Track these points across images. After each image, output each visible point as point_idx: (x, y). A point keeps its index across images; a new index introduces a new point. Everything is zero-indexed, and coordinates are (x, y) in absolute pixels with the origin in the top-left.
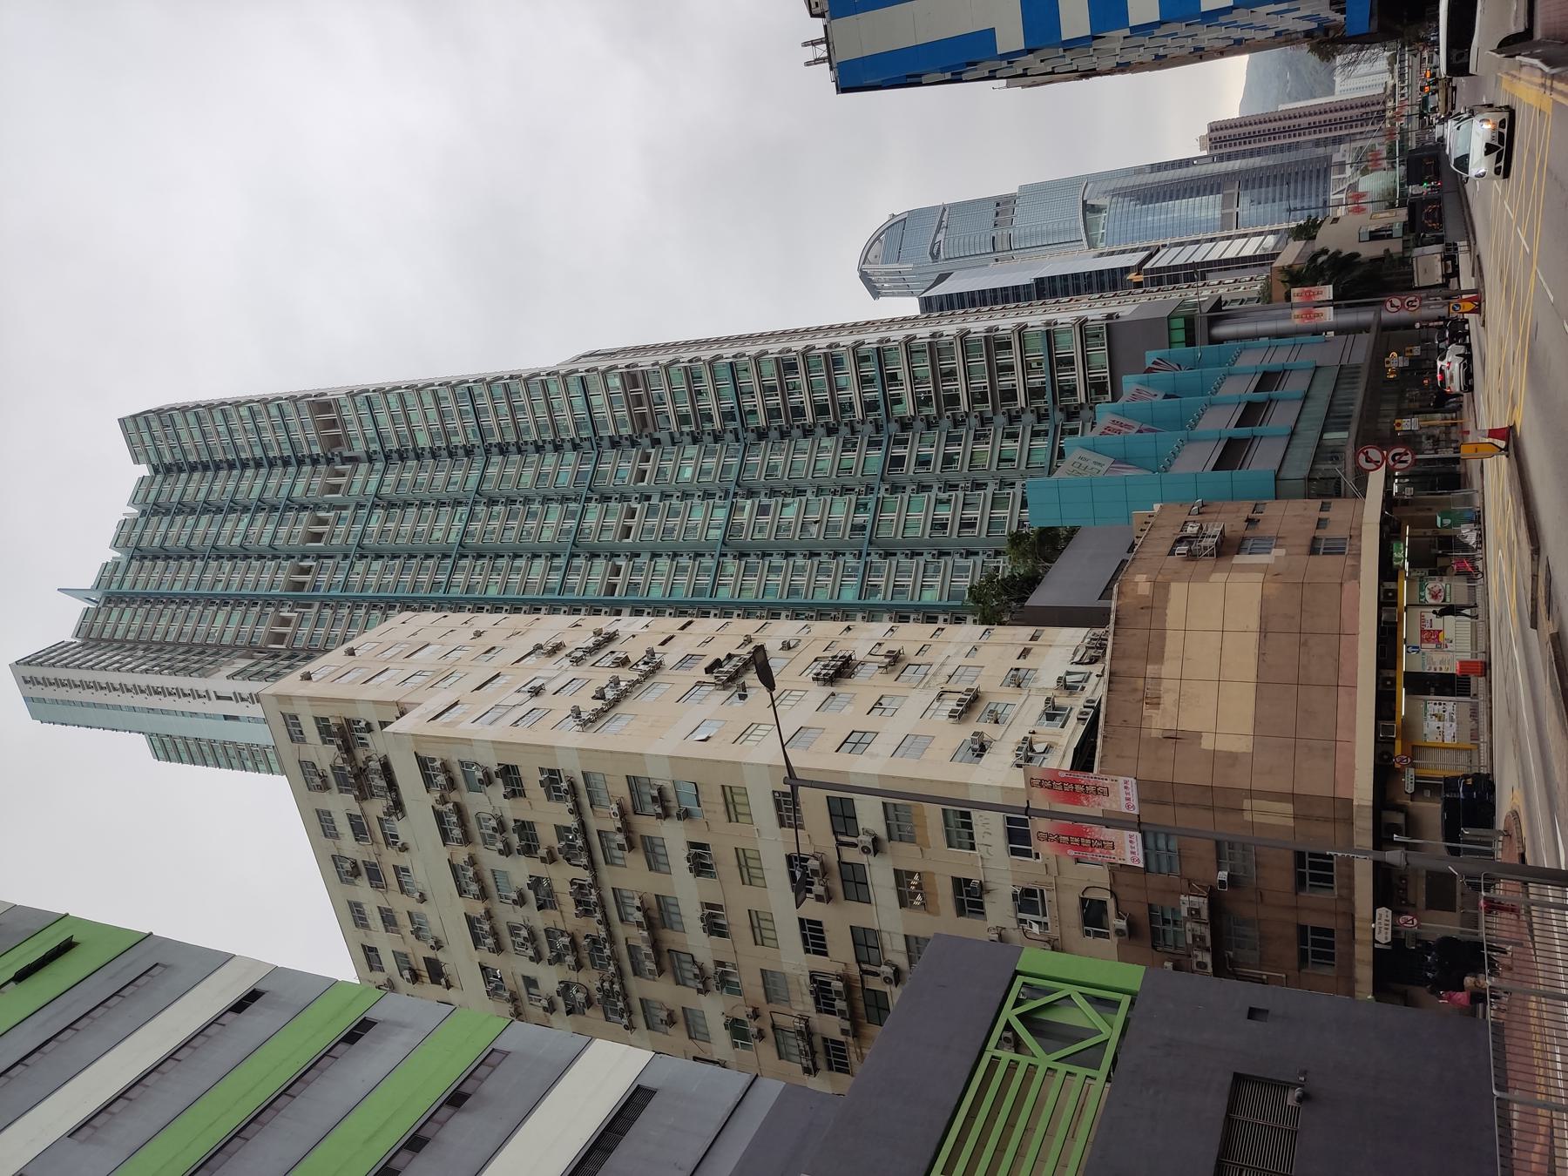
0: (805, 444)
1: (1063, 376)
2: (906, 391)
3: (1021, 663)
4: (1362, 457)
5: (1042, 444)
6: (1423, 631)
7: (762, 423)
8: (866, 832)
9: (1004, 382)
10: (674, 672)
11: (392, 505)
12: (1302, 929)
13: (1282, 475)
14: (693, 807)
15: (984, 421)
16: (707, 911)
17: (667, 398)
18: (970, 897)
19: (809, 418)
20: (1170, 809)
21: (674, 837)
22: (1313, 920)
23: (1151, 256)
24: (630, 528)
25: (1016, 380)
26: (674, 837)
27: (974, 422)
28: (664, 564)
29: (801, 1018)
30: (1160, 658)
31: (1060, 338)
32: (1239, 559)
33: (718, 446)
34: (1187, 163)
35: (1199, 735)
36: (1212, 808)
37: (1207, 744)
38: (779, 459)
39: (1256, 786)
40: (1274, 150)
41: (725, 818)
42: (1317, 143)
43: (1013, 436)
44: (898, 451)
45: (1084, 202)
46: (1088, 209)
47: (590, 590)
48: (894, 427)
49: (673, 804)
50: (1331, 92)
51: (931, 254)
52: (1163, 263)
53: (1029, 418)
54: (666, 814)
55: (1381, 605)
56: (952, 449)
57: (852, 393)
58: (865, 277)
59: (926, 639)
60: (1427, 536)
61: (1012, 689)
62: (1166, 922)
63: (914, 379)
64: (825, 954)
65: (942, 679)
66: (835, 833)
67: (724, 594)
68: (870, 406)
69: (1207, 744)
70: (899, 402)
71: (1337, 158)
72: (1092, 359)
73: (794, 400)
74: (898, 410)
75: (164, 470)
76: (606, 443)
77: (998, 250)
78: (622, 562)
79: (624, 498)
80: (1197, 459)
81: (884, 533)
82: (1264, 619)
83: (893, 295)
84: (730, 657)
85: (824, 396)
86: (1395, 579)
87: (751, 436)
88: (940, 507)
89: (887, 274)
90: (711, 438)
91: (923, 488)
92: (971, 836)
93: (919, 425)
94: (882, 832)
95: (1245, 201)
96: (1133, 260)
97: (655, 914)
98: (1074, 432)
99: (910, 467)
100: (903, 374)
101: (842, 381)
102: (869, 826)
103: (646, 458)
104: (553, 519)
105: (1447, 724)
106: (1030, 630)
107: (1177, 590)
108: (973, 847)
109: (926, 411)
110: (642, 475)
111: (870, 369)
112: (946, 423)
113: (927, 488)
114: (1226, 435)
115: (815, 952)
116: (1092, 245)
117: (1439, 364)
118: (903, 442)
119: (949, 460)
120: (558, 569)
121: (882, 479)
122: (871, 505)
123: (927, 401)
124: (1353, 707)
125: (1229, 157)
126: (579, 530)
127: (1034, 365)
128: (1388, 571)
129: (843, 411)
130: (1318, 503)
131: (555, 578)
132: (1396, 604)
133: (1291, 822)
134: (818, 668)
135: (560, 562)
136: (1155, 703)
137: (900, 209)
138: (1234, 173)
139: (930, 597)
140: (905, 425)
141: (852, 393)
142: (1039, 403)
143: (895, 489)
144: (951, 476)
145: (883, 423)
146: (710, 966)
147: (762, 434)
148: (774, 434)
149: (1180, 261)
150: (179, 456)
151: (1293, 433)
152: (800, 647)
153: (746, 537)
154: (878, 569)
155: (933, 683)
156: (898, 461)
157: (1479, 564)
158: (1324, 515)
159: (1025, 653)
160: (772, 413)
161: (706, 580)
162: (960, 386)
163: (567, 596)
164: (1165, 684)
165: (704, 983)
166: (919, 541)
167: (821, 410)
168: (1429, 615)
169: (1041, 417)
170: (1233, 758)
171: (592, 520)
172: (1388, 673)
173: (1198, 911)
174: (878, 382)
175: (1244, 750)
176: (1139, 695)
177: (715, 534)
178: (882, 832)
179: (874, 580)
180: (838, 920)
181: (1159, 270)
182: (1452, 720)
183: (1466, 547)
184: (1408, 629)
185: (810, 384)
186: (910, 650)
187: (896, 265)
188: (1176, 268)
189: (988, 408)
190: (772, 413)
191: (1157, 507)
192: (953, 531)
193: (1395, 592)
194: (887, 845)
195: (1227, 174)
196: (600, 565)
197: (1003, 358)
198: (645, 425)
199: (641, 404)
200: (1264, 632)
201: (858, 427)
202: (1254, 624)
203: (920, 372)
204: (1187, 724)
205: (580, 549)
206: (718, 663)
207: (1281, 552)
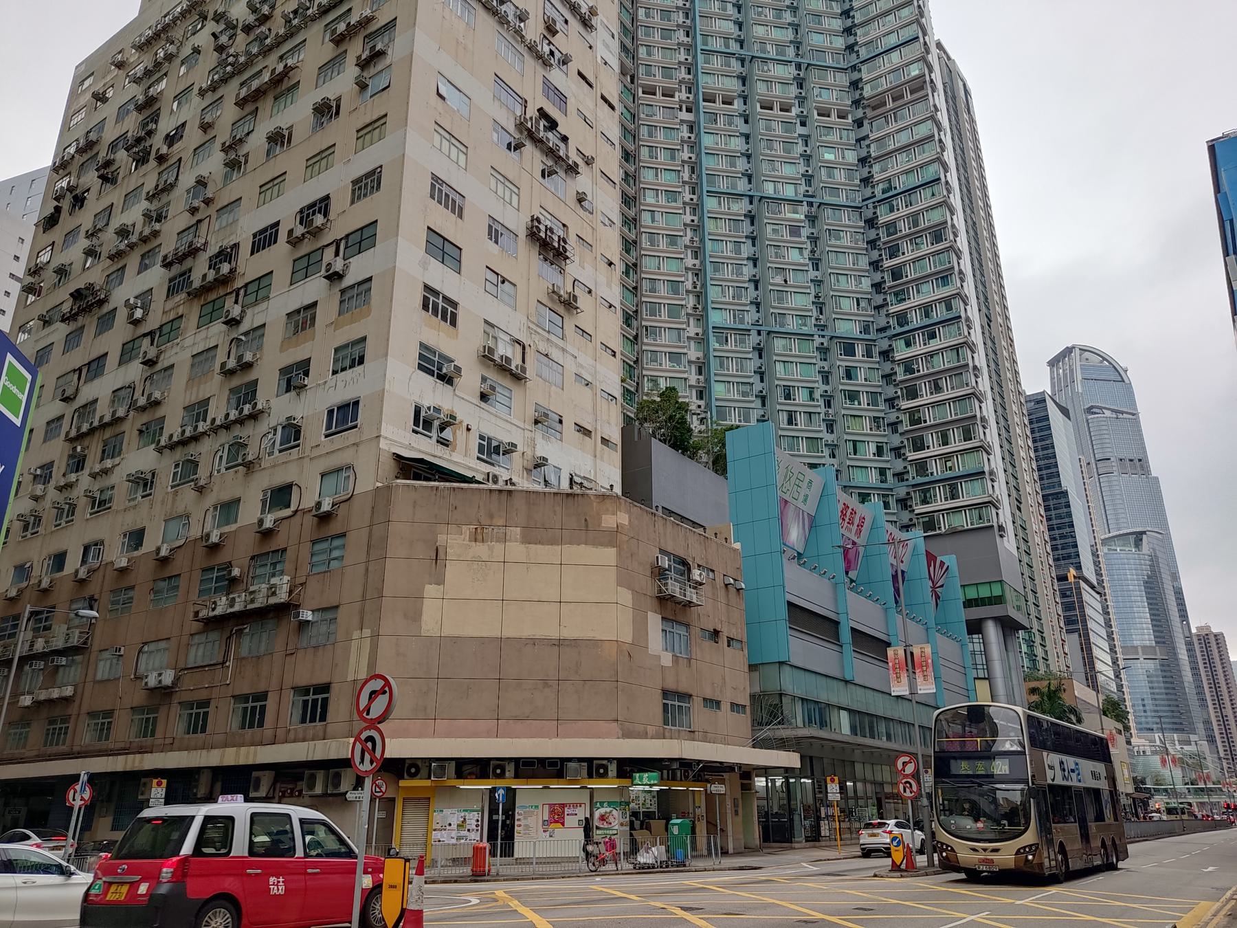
0: (864, 263)
1: (940, 492)
2: (918, 349)
3: (569, 426)
4: (907, 759)
5: (873, 478)
6: (563, 806)
7: (882, 220)
8: (346, 266)
9: (931, 439)
10: (540, 80)
12: (262, 696)
13: (787, 669)
14: (369, 92)
15: (894, 426)
16: (286, 133)
17: (901, 124)
18: (295, 377)
20: (363, 558)
21: (342, 84)
22: (271, 704)
23: (1093, 587)
24: (771, 109)
25: (934, 448)
26: (342, 84)
27: (892, 417)
28: (737, 144)
29: (206, 243)
30: (527, 540)
31: (977, 484)
32: (654, 621)
33: (857, 182)
34: (1184, 616)
35: (440, 581)
36: (364, 599)
37: (430, 590)
38: (846, 240)
39: (383, 642)
40: (1199, 687)
41: (360, 125)
42: (1207, 722)
43: (879, 451)
44: (860, 350)
45: (1144, 533)
46: (1138, 537)
47: (708, 79)
48: (884, 344)
49: (372, 71)
51: (1092, 407)
52: (1086, 597)
53: (899, 465)
54: (363, 65)
55: (590, 761)
56: (864, 399)
57: (915, 300)
58: (1069, 351)
59: (600, 337)
60: (681, 812)
61: (531, 414)
62: (274, 565)
63: (931, 355)
64: (252, 254)
65: (542, 347)
66: (347, 236)
67: (711, 204)
68: (902, 318)
69: (430, 590)
70: (908, 344)
71: (1193, 738)
72: (958, 515)
73: (905, 246)
74: (899, 344)
76: (856, 76)
77: (1097, 465)
78: (737, 105)
79: (802, 100)
80: (813, 591)
81: (779, 344)
82: (575, 643)
83: (1052, 379)
84: (565, 139)
85: (911, 273)
86: (622, 774)
87: (869, 214)
88: (806, 392)
89: (1071, 371)
90: (866, 175)
91: (826, 377)
92: (343, 369)
93: (887, 367)
94: (348, 281)
95: (1151, 665)
96: (1089, 572)
97: (286, 84)
98: (886, 505)
99: (843, 362)
100: (935, 344)
101: (924, 288)
102: (352, 268)
103: (842, 116)
104: (777, 34)
105: (454, 834)
106: (616, 437)
108: (335, 372)
109: (900, 370)
110: (824, 113)
111: (940, 313)
112: (890, 391)
113: (826, 380)
114: (842, 619)
115: (254, 243)
116: (1105, 542)
117: (892, 822)
118: (869, 354)
119: (853, 396)
120: (727, 46)
121: (832, 338)
122: (805, 330)
123: (909, 369)
124: (475, 735)
125: (1190, 650)
126: (765, 60)
127: (949, 464)
128: (628, 767)
129: (896, 294)
130: (744, 700)
131: (717, 44)
132: (590, 776)
133: (350, 678)
134: (547, 221)
135: (734, 47)
137: (1132, 376)
138: (1175, 654)
139: (719, 390)
140: (886, 354)
141: (915, 300)
142: (912, 471)
143: (824, 351)
144: (839, 399)
145: (889, 331)
146: (242, 151)
147: (871, 223)
148: (872, 234)
149: (1089, 611)
151: (847, 682)
152: (581, 212)
153: (767, 214)
154: (742, 341)
155: (536, 338)
156: (849, 350)
157: (610, 867)
158: (725, 706)
159: (584, 431)
160: (891, 227)
161: (723, 186)
163: (700, 58)
165: (230, 147)
166: (773, 377)
167: (896, 273)
168: (582, 813)
169: (900, 476)
170: (415, 616)
171: (779, 71)
172: (510, 770)
173: (274, 594)
174: (927, 322)
175: (424, 627)
177: (769, 189)
178: (348, 281)
179: (731, 340)
180: (278, 256)
181: (1079, 594)
182: (459, 838)
183: (634, 849)
184: (560, 791)
185: (921, 258)
186: (584, 320)
187: (1080, 377)
188: (1082, 608)
189: (905, 426)
190: (891, 227)
191: (737, 546)
193: (604, 775)
194: (336, 290)
195: (1174, 648)
196: (734, 85)
197: (955, 435)
198: (874, 108)
199: (894, 100)
200: (559, 643)
201: (883, 312)
202: (567, 634)
203: (938, 360)
204: (452, 571)
205: (747, 62)
206: (553, 125)
207: (667, 660)
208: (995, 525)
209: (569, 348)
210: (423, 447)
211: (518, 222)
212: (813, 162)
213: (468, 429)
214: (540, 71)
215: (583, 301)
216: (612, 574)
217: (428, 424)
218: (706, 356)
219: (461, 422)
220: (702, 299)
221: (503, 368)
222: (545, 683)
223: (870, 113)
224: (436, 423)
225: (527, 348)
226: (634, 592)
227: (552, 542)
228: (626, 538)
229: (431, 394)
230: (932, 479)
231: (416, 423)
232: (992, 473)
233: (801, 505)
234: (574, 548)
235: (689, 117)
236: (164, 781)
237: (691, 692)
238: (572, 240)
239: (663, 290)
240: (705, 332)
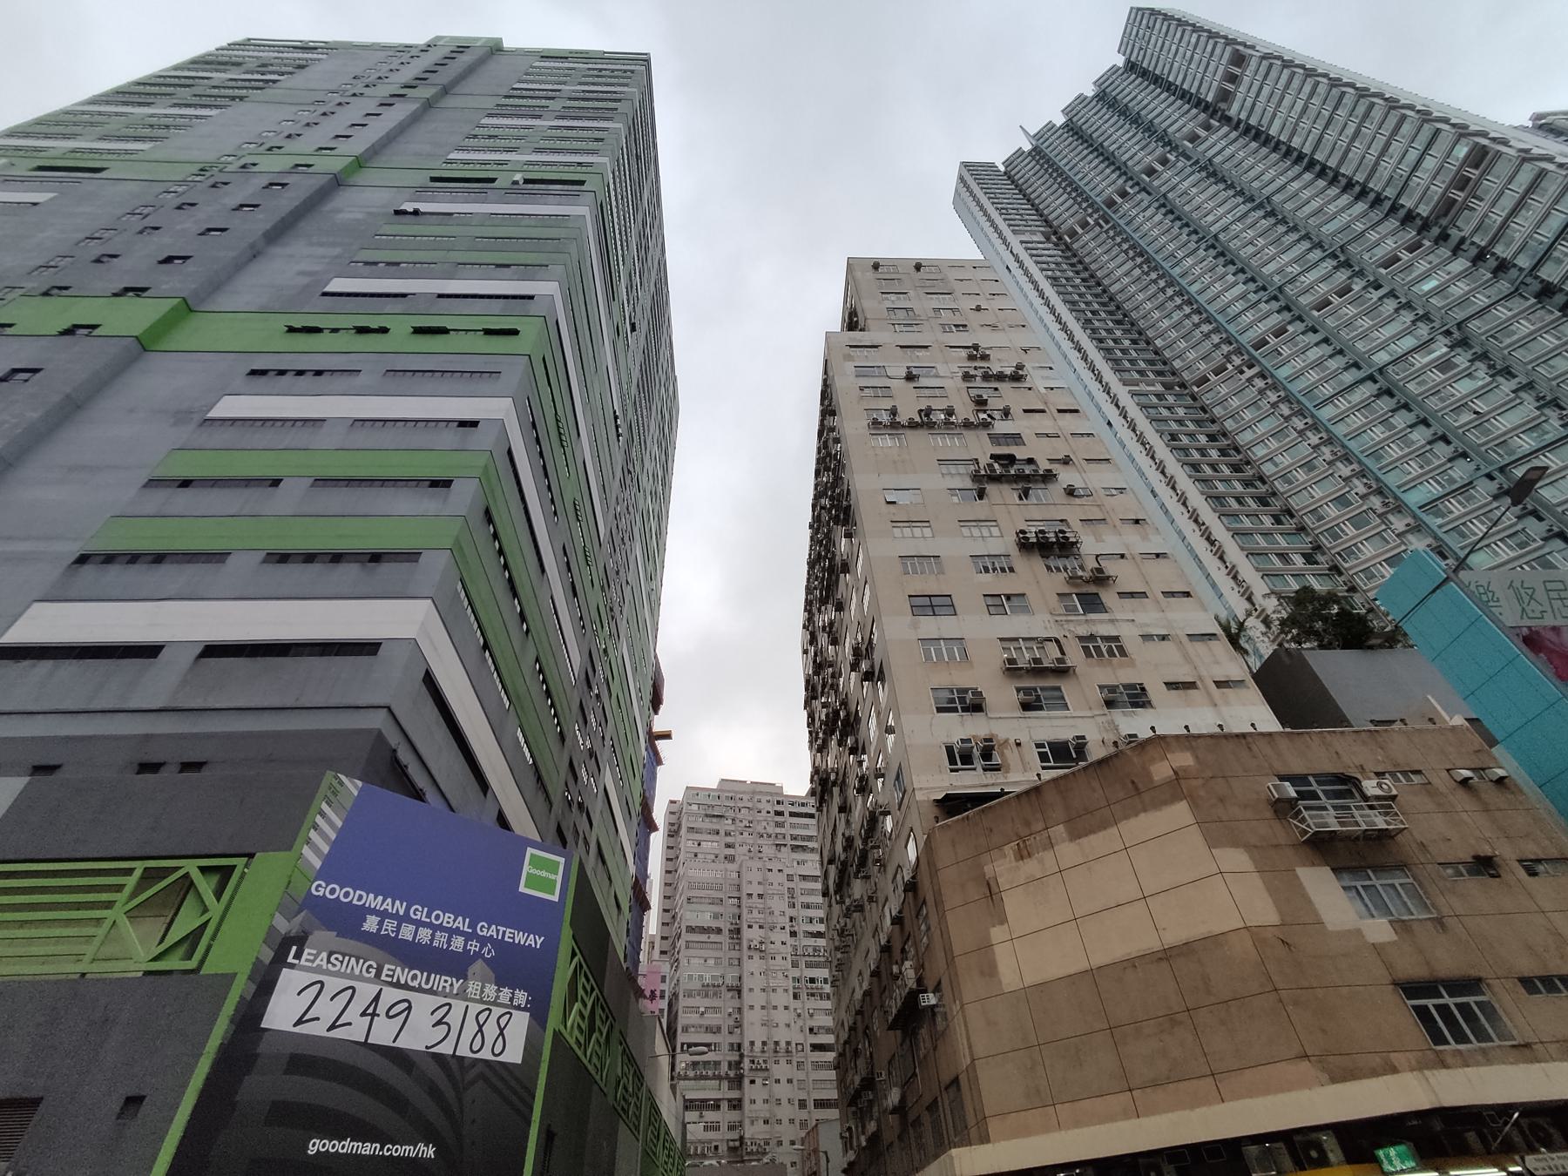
11: (1214, 174)
17: (1489, 198)
30: (1075, 835)
35: (1003, 920)
37: (997, 934)
61: (1098, 696)
67: (1326, 413)
69: (997, 934)
75: (1131, 66)
82: (1186, 949)
84: (1031, 461)
107: (1180, 812)
136: (1022, 854)
152: (1078, 501)
164: (1048, 856)
170: (990, 970)
176: (1023, 831)
200: (1166, 955)
202: (1173, 937)
206: (1011, 459)
207: (1379, 930)
210: (971, 781)
211: (1008, 544)
212: (1417, 303)
213: (1018, 745)
214: (983, 434)
215: (1110, 568)
216: (1195, 837)
217: (967, 759)
218: (1436, 537)
219: (1006, 741)
220: (1386, 491)
221: (1038, 670)
222: (1172, 1020)
223: (1444, 222)
224: (976, 753)
225: (1063, 641)
226: (1248, 847)
227: (1104, 826)
228: (1200, 782)
229: (960, 728)
231: (952, 761)
234: (1133, 822)
235: (1255, 370)
237: (1474, 973)
238: (1076, 524)
239: (1332, 511)
240: (1415, 517)
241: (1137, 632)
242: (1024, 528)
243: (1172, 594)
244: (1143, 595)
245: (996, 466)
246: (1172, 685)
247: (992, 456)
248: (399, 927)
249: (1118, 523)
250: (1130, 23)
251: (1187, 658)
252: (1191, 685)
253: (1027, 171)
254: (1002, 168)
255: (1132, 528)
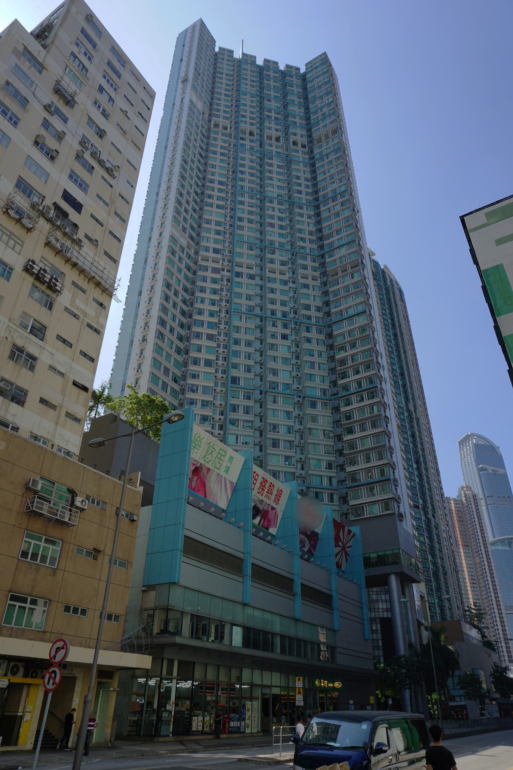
19: (340, 382)
50: (16, 744)
75: (304, 78)
84: (76, 226)
99: (310, 411)
111: (376, 476)
112: (341, 460)
121: (308, 488)
140: (336, 409)
150: (309, 79)
156: (313, 405)
162: (358, 434)
190: (346, 387)
192: (271, 435)
205: (263, 248)
208: (396, 512)
209: (47, 347)
230: (360, 484)
232: (395, 480)
233: (222, 473)
236: (301, 678)
238: (68, 283)
241: (49, 362)
242: (37, 261)
243: (85, 355)
244: (71, 345)
245: (52, 212)
246: (43, 401)
247: (55, 204)
248: (271, 690)
249: (91, 299)
250: (251, 56)
251: (63, 392)
252: (53, 407)
253: (225, 67)
254: (217, 50)
255: (95, 304)
